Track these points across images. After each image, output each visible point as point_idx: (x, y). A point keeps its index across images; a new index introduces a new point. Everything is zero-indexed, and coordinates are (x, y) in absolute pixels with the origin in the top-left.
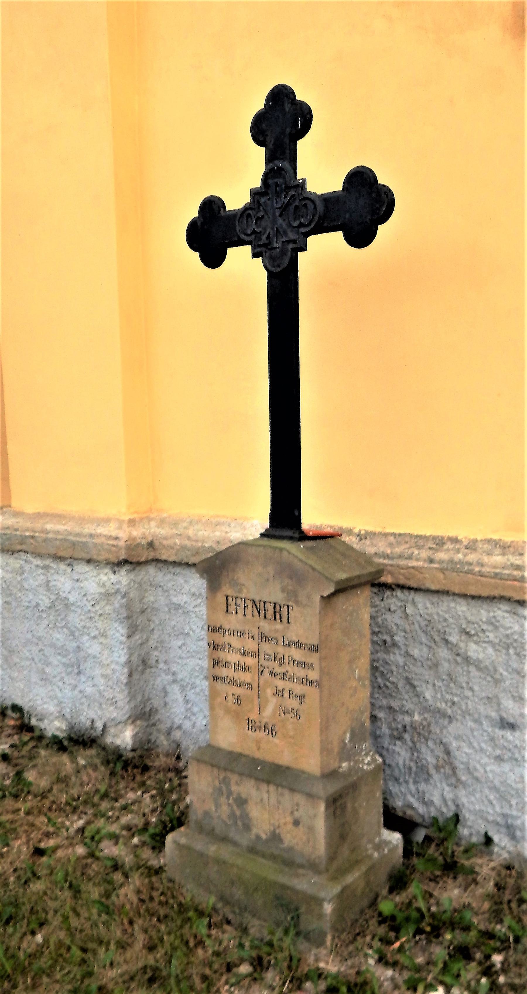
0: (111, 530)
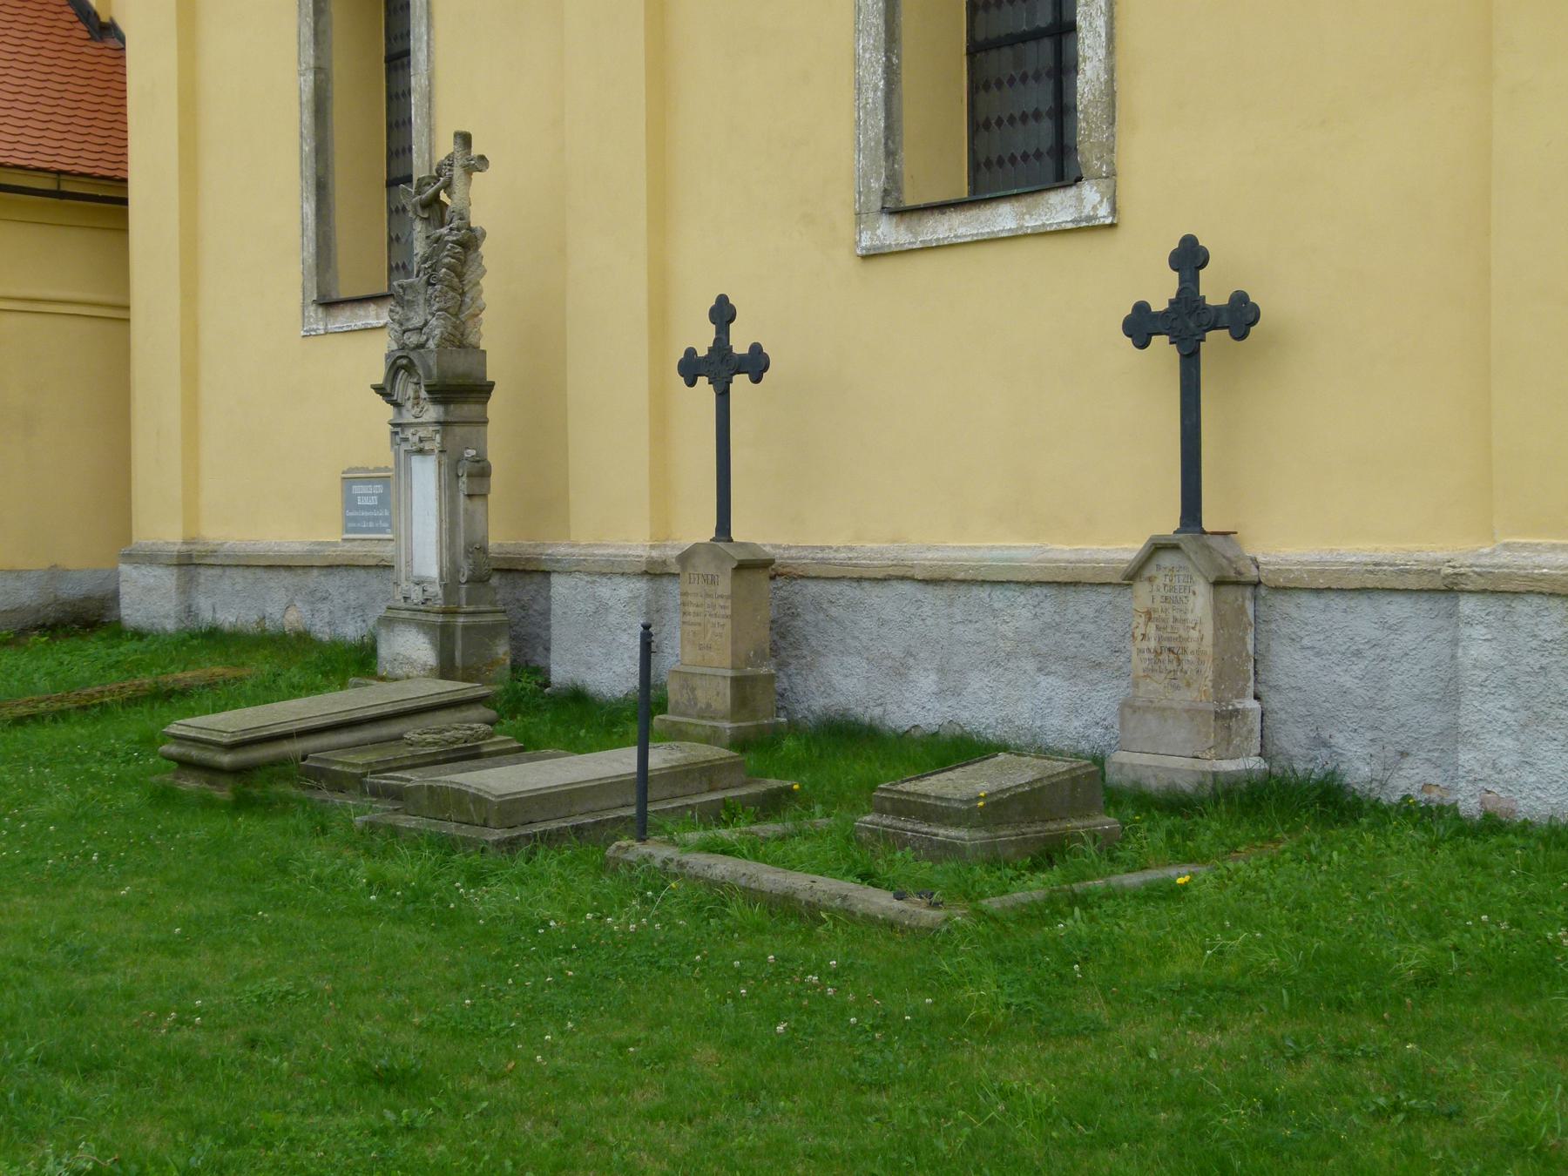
0: (639, 552)
